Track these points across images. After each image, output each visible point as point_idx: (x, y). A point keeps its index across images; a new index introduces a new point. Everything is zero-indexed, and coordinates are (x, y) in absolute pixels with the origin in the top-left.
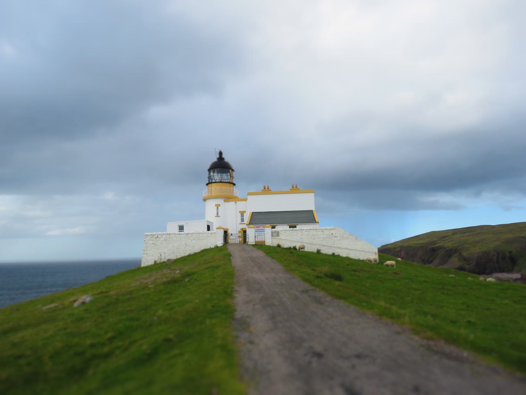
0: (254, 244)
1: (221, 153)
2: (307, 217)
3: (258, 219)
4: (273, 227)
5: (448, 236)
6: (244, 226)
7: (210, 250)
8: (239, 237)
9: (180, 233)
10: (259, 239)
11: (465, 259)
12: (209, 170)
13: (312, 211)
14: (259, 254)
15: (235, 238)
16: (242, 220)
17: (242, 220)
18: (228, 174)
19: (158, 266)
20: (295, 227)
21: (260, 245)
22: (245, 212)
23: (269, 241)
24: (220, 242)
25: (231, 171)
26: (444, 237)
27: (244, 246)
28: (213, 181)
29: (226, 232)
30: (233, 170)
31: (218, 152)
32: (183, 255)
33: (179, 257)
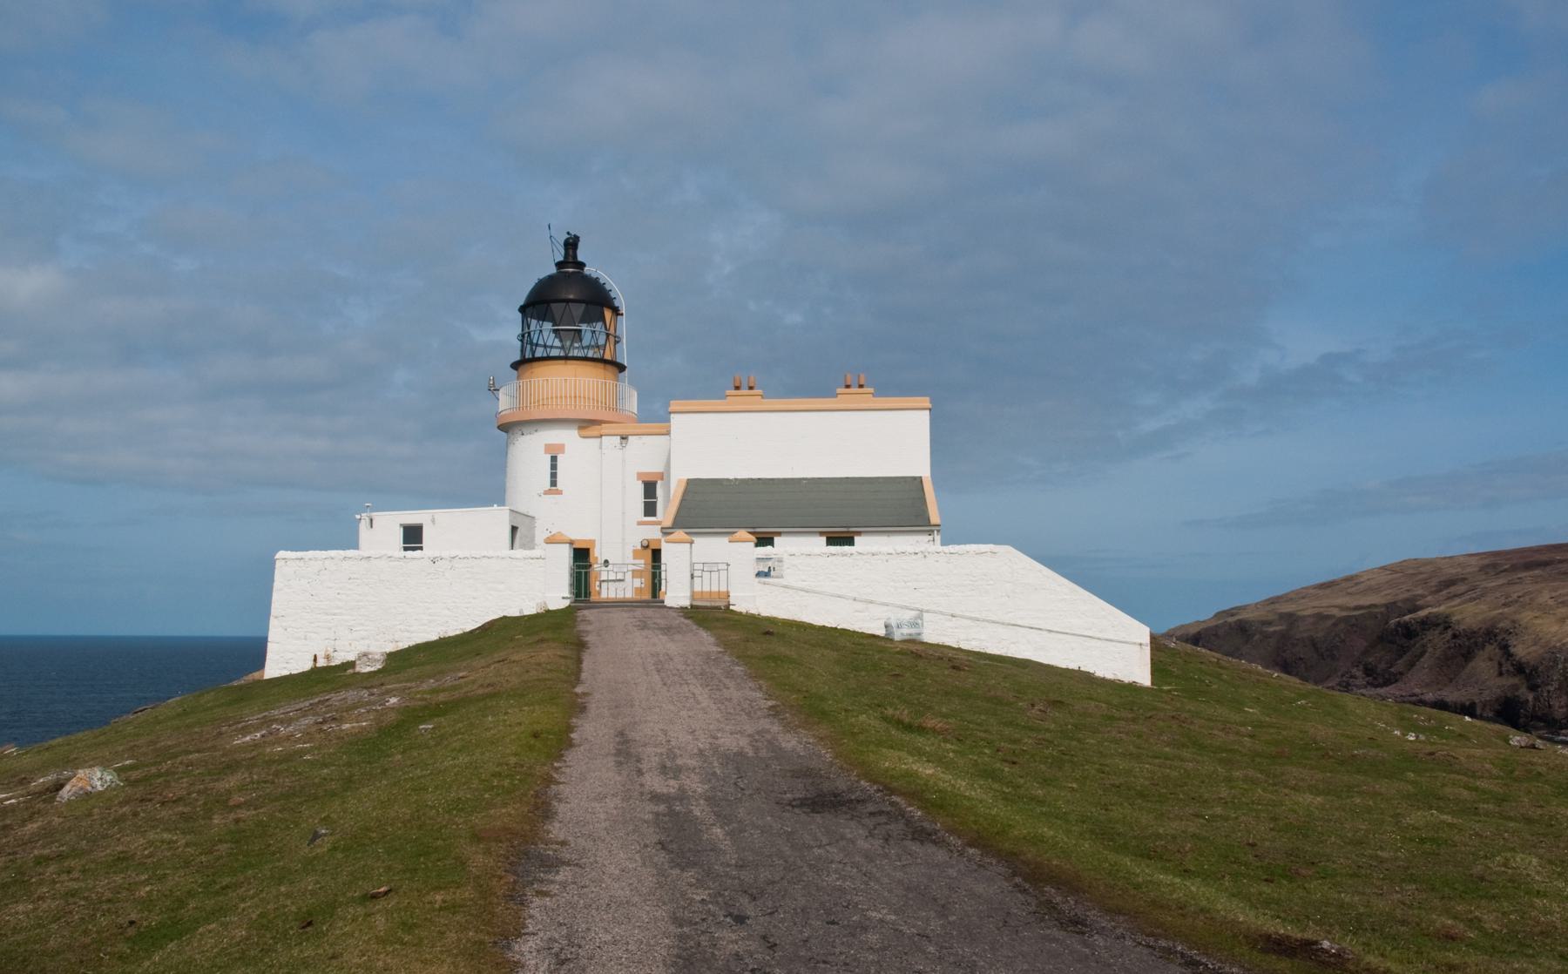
0: (687, 603)
1: (572, 244)
2: (886, 507)
3: (713, 507)
4: (764, 540)
5: (1463, 580)
6: (653, 533)
8: (636, 574)
9: (410, 553)
11: (1520, 669)
12: (523, 309)
15: (618, 579)
16: (650, 509)
18: (599, 326)
19: (401, 661)
20: (848, 540)
21: (711, 616)
23: (752, 599)
24: (558, 596)
25: (608, 314)
26: (1451, 583)
27: (649, 612)
28: (539, 352)
29: (582, 555)
30: (616, 311)
31: (563, 237)
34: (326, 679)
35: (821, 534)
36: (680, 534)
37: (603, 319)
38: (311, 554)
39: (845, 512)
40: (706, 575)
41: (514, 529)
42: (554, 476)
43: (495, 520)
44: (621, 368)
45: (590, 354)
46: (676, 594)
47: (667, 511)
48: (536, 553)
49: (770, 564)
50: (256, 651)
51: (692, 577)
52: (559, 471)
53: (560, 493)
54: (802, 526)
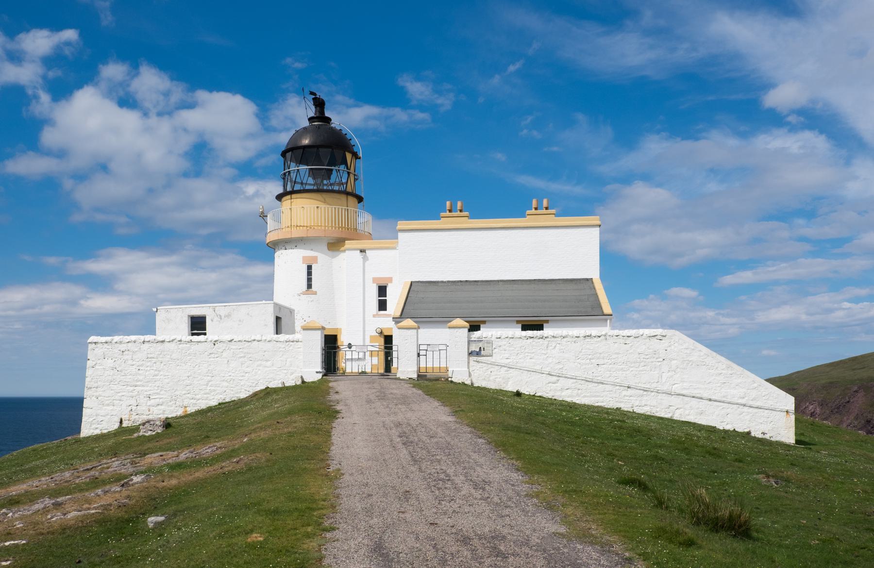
3: (429, 303)
4: (474, 327)
6: (386, 322)
7: (284, 391)
9: (195, 338)
10: (431, 363)
12: (284, 154)
13: (589, 281)
14: (435, 413)
16: (382, 305)
17: (382, 305)
20: (539, 327)
21: (432, 384)
22: (390, 280)
24: (311, 369)
27: (386, 382)
28: (297, 187)
29: (331, 343)
30: (355, 155)
32: (203, 405)
33: (191, 410)
34: (124, 440)
35: (518, 322)
36: (408, 322)
37: (344, 162)
38: (116, 338)
39: (536, 308)
40: (430, 354)
41: (278, 319)
42: (309, 273)
43: (259, 315)
44: (360, 199)
45: (336, 188)
46: (405, 366)
47: (395, 299)
48: (297, 336)
49: (481, 345)
50: (73, 407)
51: (419, 355)
52: (313, 277)
53: (315, 293)
54: (501, 319)
